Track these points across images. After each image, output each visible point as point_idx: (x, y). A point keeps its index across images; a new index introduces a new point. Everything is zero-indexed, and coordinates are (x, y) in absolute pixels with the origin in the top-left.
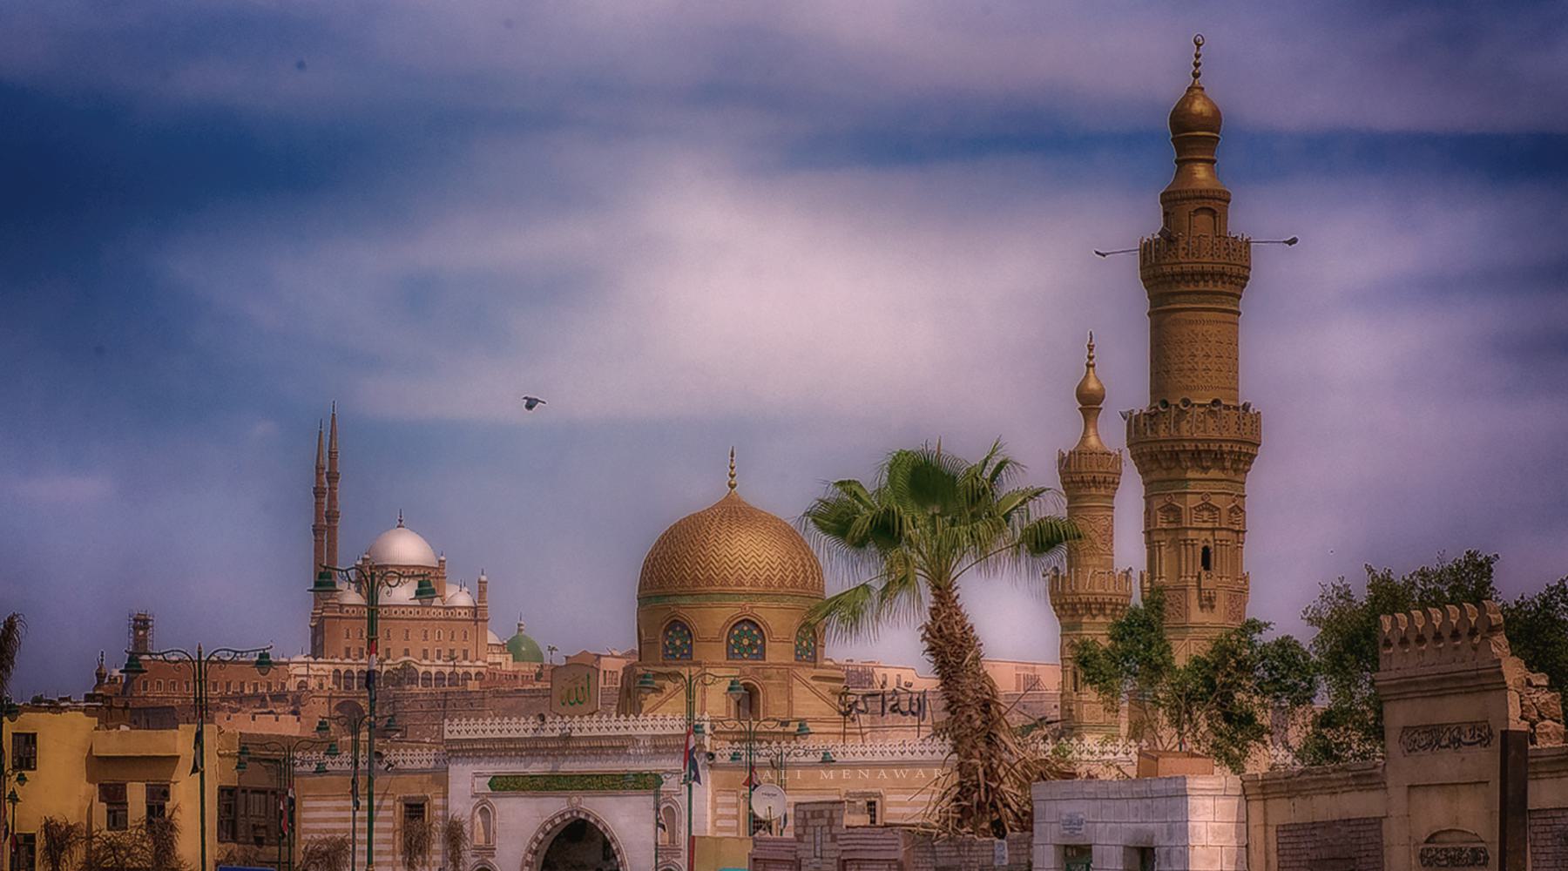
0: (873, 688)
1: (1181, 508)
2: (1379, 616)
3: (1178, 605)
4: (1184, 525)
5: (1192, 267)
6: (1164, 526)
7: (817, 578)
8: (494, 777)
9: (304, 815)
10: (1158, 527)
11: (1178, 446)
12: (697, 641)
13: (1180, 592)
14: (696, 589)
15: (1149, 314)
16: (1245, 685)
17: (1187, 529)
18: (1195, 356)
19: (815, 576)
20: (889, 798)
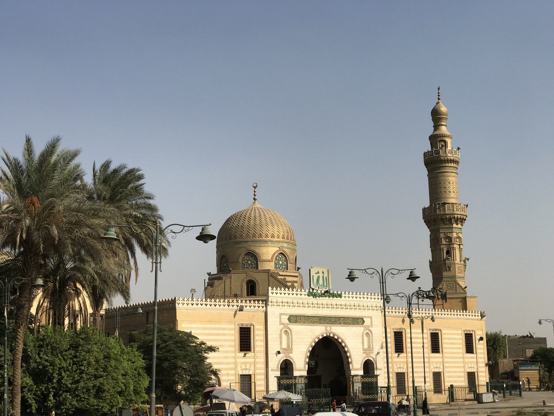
0: (132, 225)
1: (452, 237)
2: (28, 412)
3: (453, 286)
4: (453, 243)
5: (441, 138)
6: (445, 243)
7: (293, 236)
8: (290, 316)
9: (460, 337)
10: (443, 243)
11: (444, 216)
12: (260, 261)
13: (453, 282)
14: (260, 239)
15: (428, 175)
16: (56, 353)
17: (454, 244)
18: (446, 187)
19: (291, 232)
20: (443, 332)
